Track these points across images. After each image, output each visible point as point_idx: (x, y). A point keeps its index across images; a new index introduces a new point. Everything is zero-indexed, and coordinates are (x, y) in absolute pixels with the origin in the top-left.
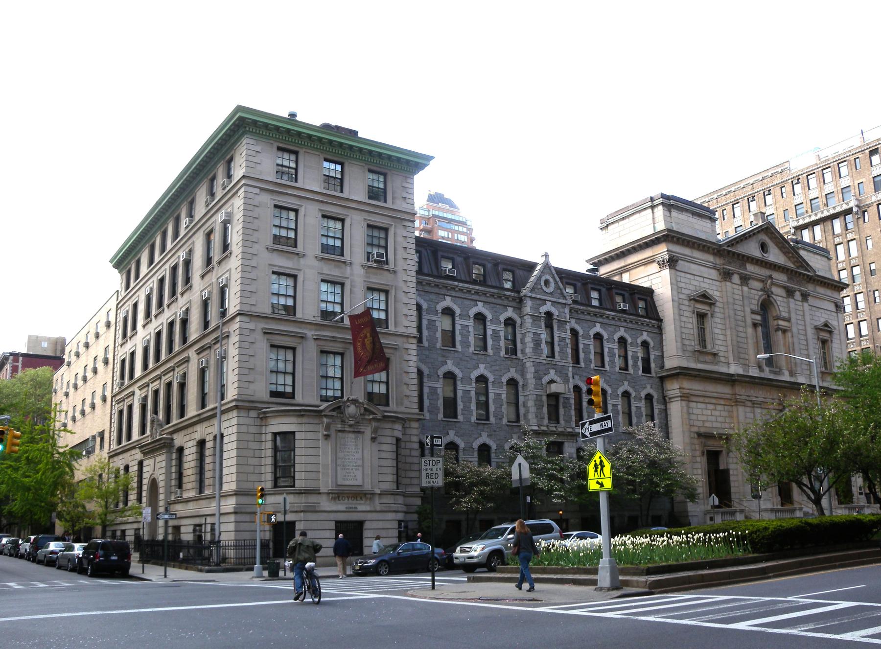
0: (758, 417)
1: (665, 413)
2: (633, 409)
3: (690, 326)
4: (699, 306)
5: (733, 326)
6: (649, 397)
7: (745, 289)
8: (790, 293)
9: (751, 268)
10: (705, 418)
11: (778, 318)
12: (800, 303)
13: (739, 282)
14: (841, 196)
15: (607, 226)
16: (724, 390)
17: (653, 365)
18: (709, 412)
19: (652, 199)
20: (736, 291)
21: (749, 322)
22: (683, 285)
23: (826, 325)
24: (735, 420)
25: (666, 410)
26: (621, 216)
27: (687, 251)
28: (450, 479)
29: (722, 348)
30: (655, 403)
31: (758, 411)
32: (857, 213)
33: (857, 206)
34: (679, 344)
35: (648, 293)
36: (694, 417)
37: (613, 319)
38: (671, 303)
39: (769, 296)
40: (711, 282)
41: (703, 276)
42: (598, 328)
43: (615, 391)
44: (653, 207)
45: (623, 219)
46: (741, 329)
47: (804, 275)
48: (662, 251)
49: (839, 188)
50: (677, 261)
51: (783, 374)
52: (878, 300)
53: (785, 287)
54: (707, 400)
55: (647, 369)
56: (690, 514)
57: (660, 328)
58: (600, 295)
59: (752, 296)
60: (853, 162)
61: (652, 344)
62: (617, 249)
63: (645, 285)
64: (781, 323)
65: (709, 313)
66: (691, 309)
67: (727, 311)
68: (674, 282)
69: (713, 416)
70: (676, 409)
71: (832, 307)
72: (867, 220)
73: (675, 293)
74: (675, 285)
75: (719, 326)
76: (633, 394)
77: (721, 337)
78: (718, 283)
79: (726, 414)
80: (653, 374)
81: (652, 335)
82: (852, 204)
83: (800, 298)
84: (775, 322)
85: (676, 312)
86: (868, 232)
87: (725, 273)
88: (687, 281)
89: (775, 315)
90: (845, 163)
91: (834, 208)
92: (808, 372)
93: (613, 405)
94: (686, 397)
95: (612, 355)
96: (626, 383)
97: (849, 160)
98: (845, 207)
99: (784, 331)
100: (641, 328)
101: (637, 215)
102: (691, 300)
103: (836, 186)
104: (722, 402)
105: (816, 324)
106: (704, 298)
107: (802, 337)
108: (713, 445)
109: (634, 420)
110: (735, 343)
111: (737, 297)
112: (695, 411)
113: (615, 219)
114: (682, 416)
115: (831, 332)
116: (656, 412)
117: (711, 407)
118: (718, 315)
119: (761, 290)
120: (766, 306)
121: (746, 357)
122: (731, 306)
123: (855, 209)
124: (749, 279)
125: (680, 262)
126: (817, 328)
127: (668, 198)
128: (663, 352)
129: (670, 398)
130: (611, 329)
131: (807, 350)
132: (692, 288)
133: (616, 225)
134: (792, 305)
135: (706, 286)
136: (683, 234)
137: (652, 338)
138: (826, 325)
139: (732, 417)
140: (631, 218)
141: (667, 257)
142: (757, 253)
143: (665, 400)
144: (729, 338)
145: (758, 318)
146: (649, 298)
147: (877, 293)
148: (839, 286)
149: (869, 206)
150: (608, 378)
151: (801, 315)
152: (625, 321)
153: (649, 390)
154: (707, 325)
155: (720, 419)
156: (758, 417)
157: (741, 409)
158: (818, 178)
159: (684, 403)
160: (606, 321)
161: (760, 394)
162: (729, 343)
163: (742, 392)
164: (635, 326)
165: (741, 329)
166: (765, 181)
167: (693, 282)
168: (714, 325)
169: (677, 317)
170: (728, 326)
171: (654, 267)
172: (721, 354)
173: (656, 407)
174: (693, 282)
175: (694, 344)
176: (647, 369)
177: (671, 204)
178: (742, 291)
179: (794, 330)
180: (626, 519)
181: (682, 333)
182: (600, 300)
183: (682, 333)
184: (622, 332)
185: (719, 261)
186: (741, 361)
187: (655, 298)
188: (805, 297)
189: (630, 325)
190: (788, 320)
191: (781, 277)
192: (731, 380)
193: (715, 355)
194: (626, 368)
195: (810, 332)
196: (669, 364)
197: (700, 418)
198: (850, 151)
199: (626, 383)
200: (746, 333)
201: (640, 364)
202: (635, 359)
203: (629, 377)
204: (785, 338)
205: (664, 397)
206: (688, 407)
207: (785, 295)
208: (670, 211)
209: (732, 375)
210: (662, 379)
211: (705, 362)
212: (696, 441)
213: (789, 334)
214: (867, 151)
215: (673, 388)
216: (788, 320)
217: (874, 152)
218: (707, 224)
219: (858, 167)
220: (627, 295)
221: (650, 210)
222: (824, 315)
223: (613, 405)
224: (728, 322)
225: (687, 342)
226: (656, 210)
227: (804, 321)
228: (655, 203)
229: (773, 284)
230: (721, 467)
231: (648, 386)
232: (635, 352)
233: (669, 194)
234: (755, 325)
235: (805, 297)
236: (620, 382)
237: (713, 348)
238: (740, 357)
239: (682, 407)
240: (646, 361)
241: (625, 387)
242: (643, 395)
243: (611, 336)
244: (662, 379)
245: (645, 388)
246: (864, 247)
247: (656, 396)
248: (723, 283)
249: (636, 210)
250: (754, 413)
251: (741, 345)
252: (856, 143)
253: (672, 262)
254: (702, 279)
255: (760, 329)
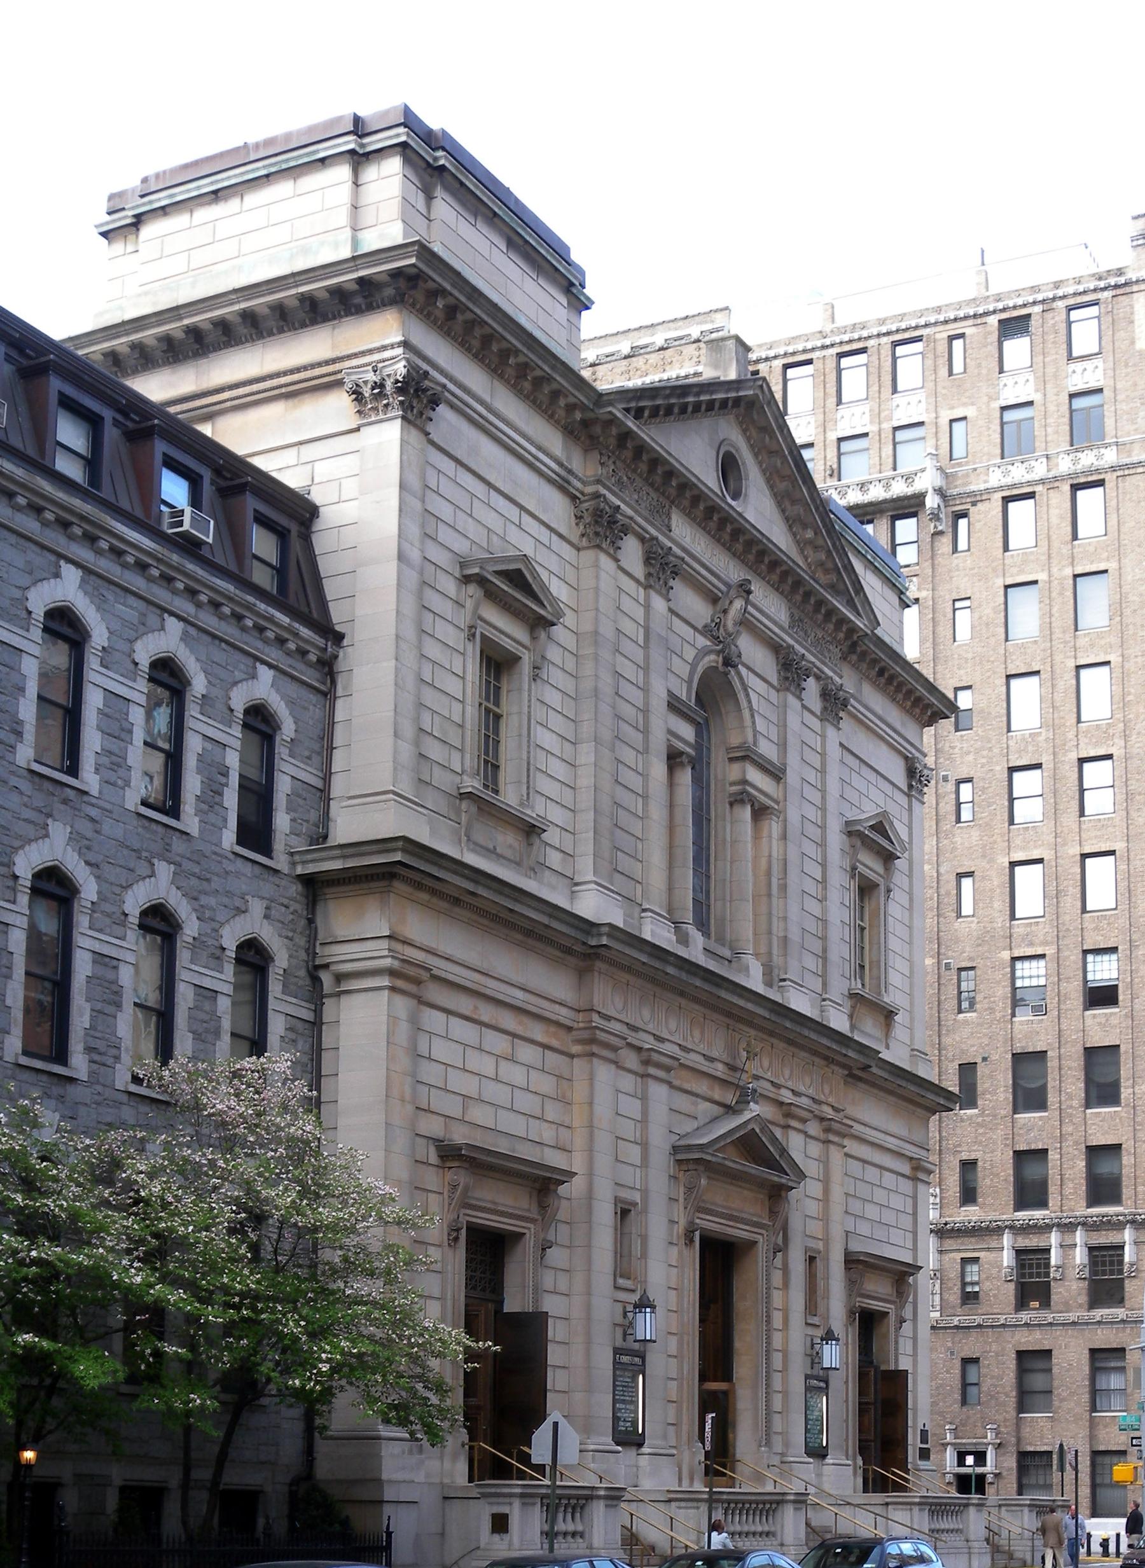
0: (659, 1114)
1: (312, 1034)
2: (185, 997)
3: (453, 686)
4: (494, 615)
5: (606, 735)
6: (253, 958)
7: (659, 604)
8: (791, 672)
9: (685, 535)
10: (470, 1086)
11: (746, 755)
12: (815, 724)
13: (639, 571)
14: (888, 450)
15: (138, 221)
16: (548, 982)
17: (282, 821)
18: (486, 1065)
19: (359, 127)
20: (627, 604)
21: (659, 741)
22: (445, 511)
23: (880, 828)
24: (578, 1119)
25: (316, 1025)
26: (206, 186)
27: (472, 376)
28: (721, 1396)
29: (556, 815)
30: (275, 988)
31: (658, 1092)
32: (935, 517)
33: (940, 492)
34: (407, 751)
35: (293, 515)
36: (430, 1073)
37: (142, 567)
38: (392, 567)
39: (728, 662)
40: (544, 535)
41: (524, 511)
42: (67, 588)
43: (112, 893)
44: (359, 159)
45: (216, 196)
46: (629, 756)
47: (844, 620)
48: (380, 339)
49: (887, 426)
50: (434, 402)
51: (746, 970)
52: (966, 815)
53: (776, 648)
54: (487, 1013)
55: (256, 833)
56: (389, 1494)
57: (328, 667)
58: (96, 442)
59: (675, 642)
60: (942, 347)
61: (288, 729)
62: (175, 312)
63: (293, 480)
64: (755, 776)
65: (526, 657)
66: (464, 618)
67: (588, 669)
68: (415, 483)
69: (504, 1090)
70: (363, 1023)
71: (896, 771)
72: (962, 544)
73: (414, 531)
74: (414, 491)
75: (556, 721)
76: (191, 928)
77: (558, 769)
78: (567, 551)
79: (546, 1084)
80: (280, 861)
81: (293, 689)
82: (926, 482)
83: (816, 704)
84: (734, 772)
85: (410, 608)
86: (964, 585)
87: (598, 514)
88: (463, 501)
89: (735, 740)
90: (918, 347)
91: (863, 486)
92: (817, 985)
93: (99, 958)
94: (410, 979)
95: (118, 731)
96: (164, 871)
97: (931, 340)
98: (899, 489)
99: (760, 812)
100: (252, 644)
101: (283, 189)
102: (466, 579)
103: (878, 416)
104: (538, 1032)
105: (852, 815)
106: (511, 587)
107: (811, 849)
108: (501, 1206)
109: (183, 1043)
110: (606, 803)
111: (628, 627)
112: (441, 1049)
113: (181, 194)
114: (390, 1058)
115: (888, 858)
116: (276, 1026)
117: (500, 1043)
118: (556, 676)
119: (706, 631)
120: (712, 697)
121: (637, 870)
122: (606, 654)
123: (932, 501)
124: (675, 573)
125: (442, 409)
126: (852, 832)
127: (433, 140)
128: (327, 776)
129: (339, 978)
130: (129, 610)
131: (822, 900)
132: (480, 536)
133: (177, 222)
134: (793, 721)
135: (528, 549)
136: (475, 293)
137: (291, 703)
138: (880, 828)
139: (565, 1102)
140: (254, 199)
141: (400, 369)
142: (708, 476)
143: (316, 981)
144: (585, 780)
145: (687, 731)
146: (294, 528)
147: (966, 791)
148: (927, 704)
149: (976, 498)
150: (86, 828)
151: (826, 769)
152: (192, 593)
153: (254, 923)
154: (514, 705)
155: (526, 1102)
156: (659, 1114)
157: (604, 1073)
158: (820, 380)
159: (402, 1004)
160: (105, 565)
161: (671, 1029)
162: (586, 800)
163: (611, 1000)
164: (227, 630)
165: (629, 756)
166: (638, 362)
167: (480, 511)
168: (539, 712)
169: (410, 633)
170: (586, 729)
171: (336, 408)
172: (552, 836)
173: (279, 993)
174: (480, 511)
175: (459, 767)
176: (256, 833)
177: (437, 165)
178: (647, 607)
179: (793, 815)
180: (112, 1502)
181: (420, 705)
182: (92, 463)
183: (420, 705)
184: (168, 640)
185: (585, 467)
186: (619, 882)
187: (321, 543)
188: (834, 704)
189: (208, 619)
190: (776, 774)
191: (771, 606)
192: (581, 947)
193: (531, 831)
194: (170, 803)
195: (836, 839)
196: (350, 825)
197: (459, 1082)
198: (939, 310)
199: (164, 871)
200: (645, 776)
201: (231, 799)
202: (215, 774)
203: (178, 846)
204: (757, 837)
205: (314, 971)
206: (417, 1028)
207: (774, 678)
208: (429, 198)
209: (588, 926)
210: (315, 887)
211: (491, 853)
212: (432, 1179)
213: (773, 827)
214: (993, 320)
215: (361, 932)
216: (776, 774)
217: (1014, 325)
218: (554, 302)
219: (958, 367)
220: (207, 489)
221: (343, 172)
222: (874, 794)
223: (99, 958)
224: (587, 716)
225: (435, 751)
226: (371, 173)
227: (823, 792)
228: (374, 142)
229: (745, 623)
230: (511, 1305)
231: (257, 907)
232: (214, 741)
233: (434, 122)
234: (674, 759)
235: (834, 704)
236: (141, 862)
237: (527, 800)
238: (615, 874)
239: (392, 1019)
240: (258, 799)
241: (159, 886)
242: (230, 940)
243: (128, 641)
244: (315, 887)
245: (241, 911)
246: (944, 631)
247: (281, 960)
248: (589, 555)
249: (286, 161)
250: (644, 1099)
251: (624, 818)
252: (955, 289)
253: (417, 397)
254: (513, 512)
255: (685, 777)
